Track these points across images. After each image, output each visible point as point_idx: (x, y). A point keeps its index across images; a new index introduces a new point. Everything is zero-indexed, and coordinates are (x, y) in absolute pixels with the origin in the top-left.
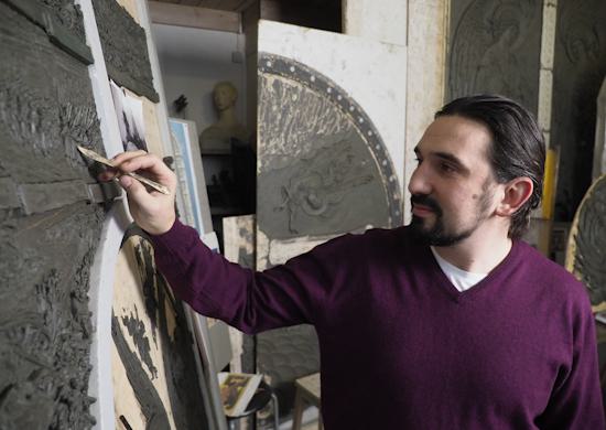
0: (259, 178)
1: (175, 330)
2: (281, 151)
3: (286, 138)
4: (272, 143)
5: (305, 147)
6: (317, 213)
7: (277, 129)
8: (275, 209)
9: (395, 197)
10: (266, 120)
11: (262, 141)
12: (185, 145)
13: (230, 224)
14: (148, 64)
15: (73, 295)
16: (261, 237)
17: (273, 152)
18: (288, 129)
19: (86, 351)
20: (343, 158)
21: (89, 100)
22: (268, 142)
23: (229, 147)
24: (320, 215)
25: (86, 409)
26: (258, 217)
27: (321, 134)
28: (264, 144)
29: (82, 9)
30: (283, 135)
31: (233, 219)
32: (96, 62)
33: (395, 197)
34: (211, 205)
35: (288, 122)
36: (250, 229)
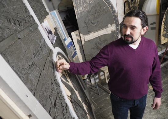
0: (77, 20)
1: (55, 32)
2: (82, 11)
3: (82, 7)
4: (79, 10)
5: (88, 8)
6: (95, 25)
7: (79, 5)
8: (83, 27)
9: (115, 15)
10: (76, 4)
11: (76, 10)
12: (57, 17)
13: (73, 34)
14: (43, 5)
15: (55, 80)
16: (82, 35)
17: (80, 12)
18: (82, 5)
19: (60, 89)
20: (99, 8)
21: (41, 36)
22: (77, 10)
23: (66, 8)
24: (96, 26)
25: (63, 98)
26: (80, 30)
27: (91, 3)
28: (77, 11)
29: (33, 16)
30: (81, 6)
31: (73, 32)
32: (39, 26)
33: (115, 15)
34: (65, 26)
35: (82, 2)
36: (78, 34)
